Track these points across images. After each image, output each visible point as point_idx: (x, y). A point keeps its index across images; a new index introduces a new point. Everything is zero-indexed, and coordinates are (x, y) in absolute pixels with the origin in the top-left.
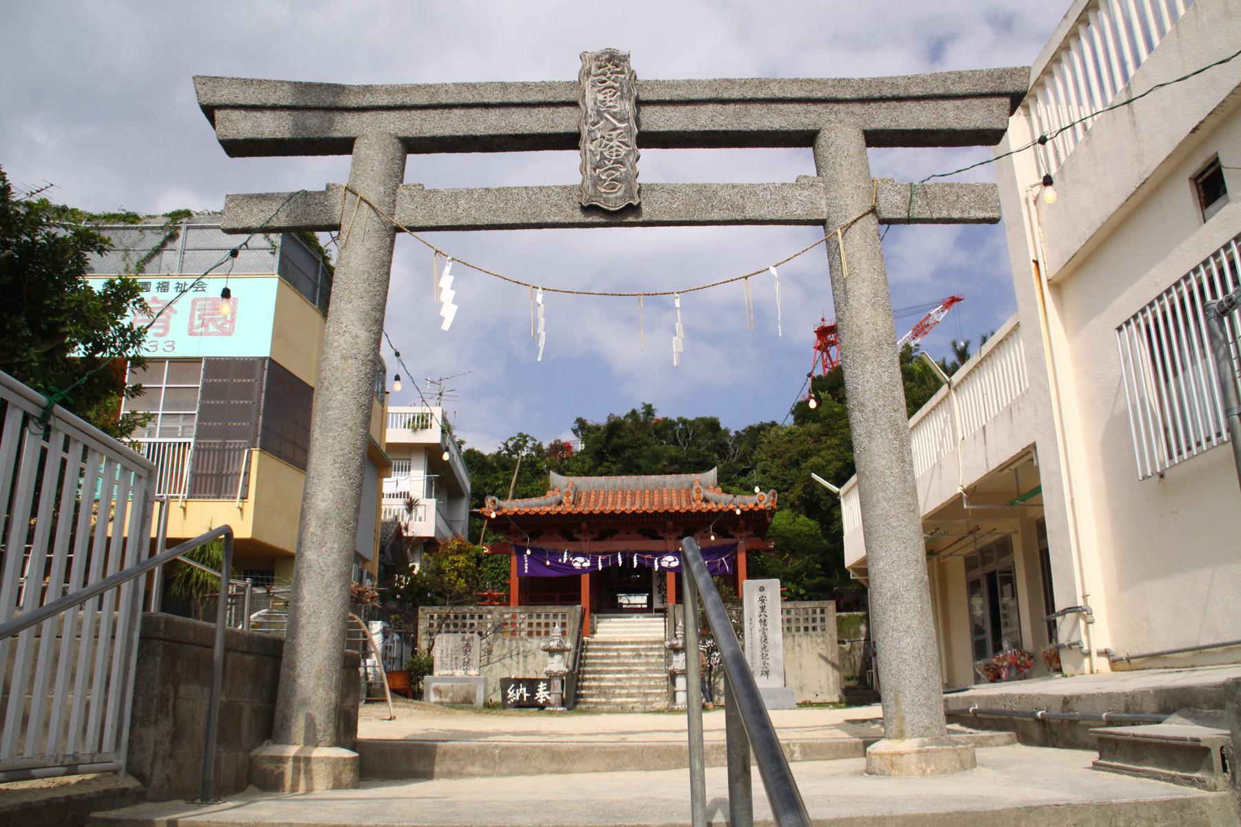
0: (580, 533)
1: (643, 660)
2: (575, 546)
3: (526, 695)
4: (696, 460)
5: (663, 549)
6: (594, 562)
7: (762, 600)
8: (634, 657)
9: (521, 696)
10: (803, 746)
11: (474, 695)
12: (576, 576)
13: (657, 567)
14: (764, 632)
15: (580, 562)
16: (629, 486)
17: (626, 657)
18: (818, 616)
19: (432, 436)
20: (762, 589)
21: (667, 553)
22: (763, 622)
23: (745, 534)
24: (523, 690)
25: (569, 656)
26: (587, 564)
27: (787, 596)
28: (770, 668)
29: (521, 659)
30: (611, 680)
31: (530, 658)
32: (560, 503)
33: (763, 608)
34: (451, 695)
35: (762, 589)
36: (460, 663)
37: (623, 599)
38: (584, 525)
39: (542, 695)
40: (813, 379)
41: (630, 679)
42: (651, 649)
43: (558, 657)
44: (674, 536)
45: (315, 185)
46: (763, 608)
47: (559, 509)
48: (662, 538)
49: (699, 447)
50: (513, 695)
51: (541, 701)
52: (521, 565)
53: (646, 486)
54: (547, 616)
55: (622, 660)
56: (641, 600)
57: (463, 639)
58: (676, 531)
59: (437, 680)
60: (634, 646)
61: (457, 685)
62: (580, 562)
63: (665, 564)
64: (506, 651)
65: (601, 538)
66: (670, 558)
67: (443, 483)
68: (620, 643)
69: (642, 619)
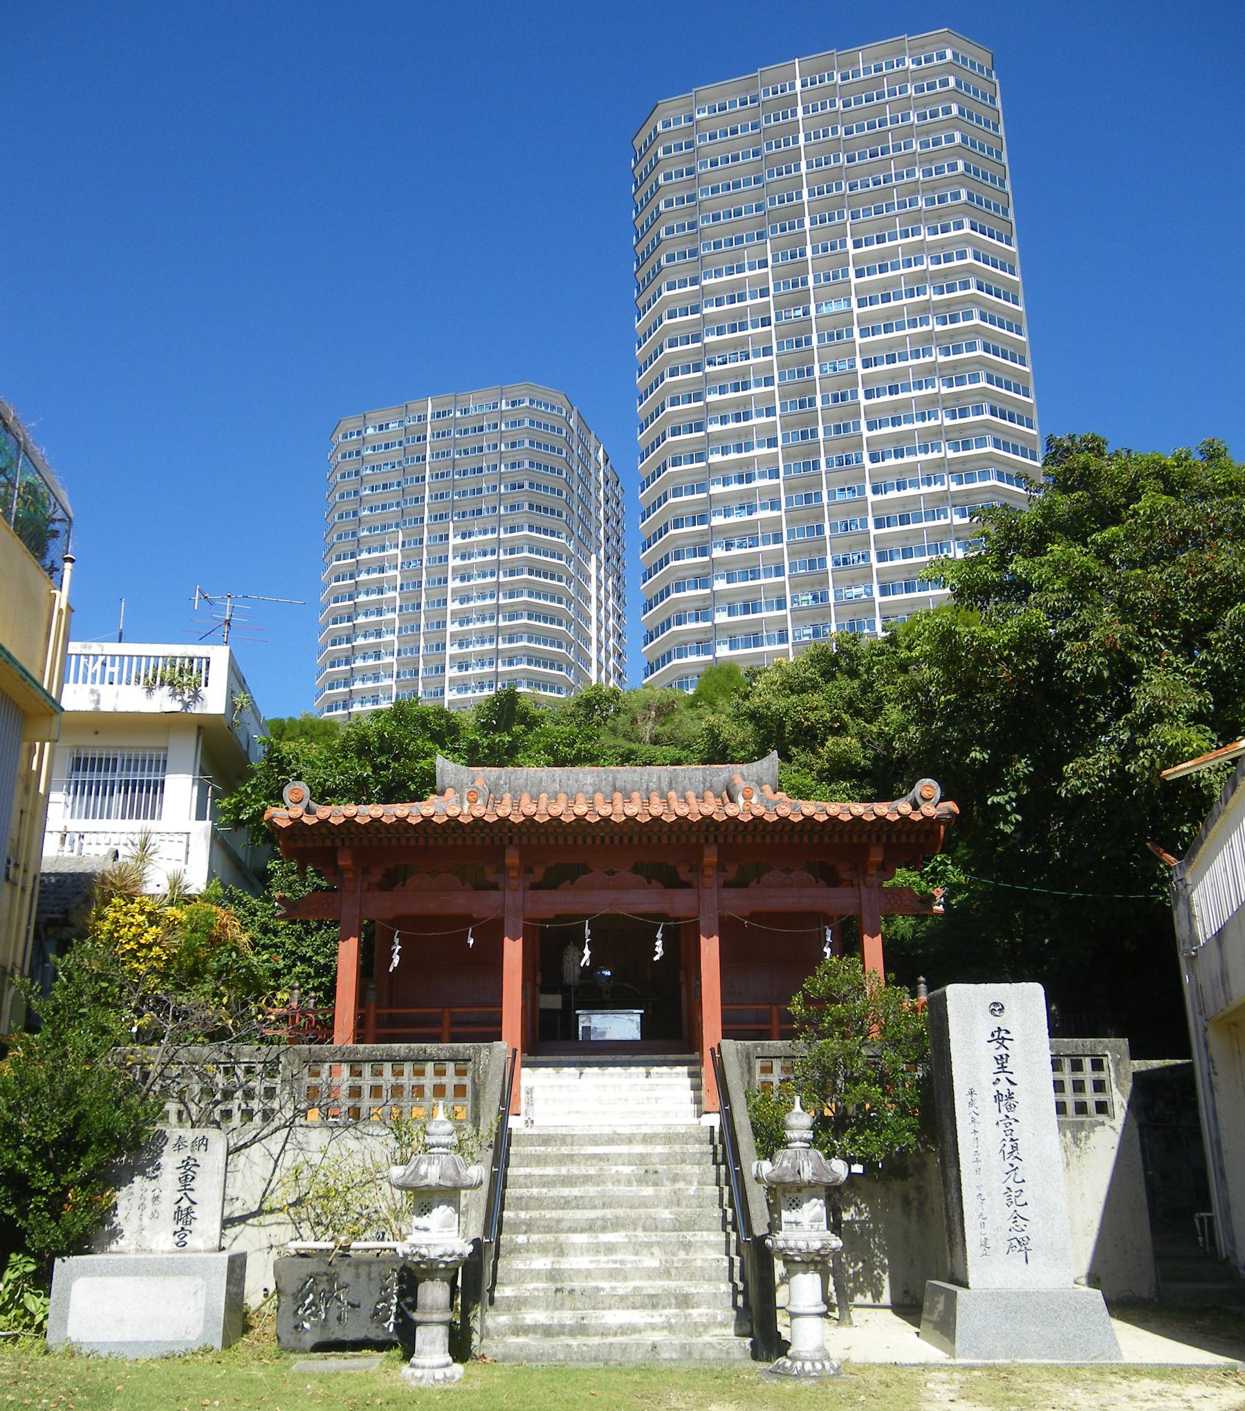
1: (666, 1189)
8: (642, 1181)
14: (1008, 1123)
18: (1088, 1075)
19: (214, 701)
20: (997, 1008)
22: (1005, 1099)
25: (474, 1203)
27: (1063, 1023)
33: (1002, 1061)
35: (997, 1008)
43: (442, 1213)
45: (613, 1240)
46: (1002, 1061)
60: (638, 1149)
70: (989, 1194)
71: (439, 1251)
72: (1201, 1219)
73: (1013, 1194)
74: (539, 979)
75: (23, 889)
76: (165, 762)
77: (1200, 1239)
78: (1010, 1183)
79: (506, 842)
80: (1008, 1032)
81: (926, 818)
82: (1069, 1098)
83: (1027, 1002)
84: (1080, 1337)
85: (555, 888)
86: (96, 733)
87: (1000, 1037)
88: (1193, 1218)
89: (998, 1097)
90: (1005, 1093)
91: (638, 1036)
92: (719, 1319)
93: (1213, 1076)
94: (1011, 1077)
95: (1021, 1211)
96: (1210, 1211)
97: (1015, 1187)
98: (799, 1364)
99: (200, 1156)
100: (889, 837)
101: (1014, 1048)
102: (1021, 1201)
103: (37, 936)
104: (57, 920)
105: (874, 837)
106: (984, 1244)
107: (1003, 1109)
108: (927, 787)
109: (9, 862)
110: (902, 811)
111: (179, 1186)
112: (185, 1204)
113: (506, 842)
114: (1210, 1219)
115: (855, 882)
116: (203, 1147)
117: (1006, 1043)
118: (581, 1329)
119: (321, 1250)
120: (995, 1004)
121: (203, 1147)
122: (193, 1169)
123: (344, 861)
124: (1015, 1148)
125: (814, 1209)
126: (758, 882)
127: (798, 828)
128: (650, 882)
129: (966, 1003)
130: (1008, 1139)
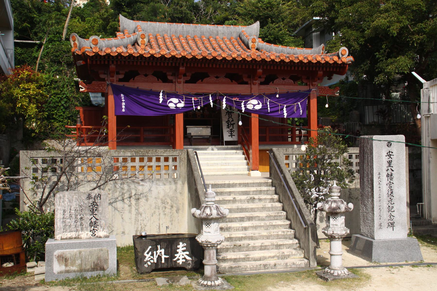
2: (168, 87)
3: (163, 257)
4: (179, 16)
5: (248, 93)
6: (188, 102)
7: (389, 154)
8: (248, 201)
9: (159, 258)
10: (212, 184)
11: (106, 260)
12: (171, 115)
13: (243, 109)
14: (390, 185)
15: (174, 103)
16: (188, 32)
17: (241, 201)
20: (389, 144)
21: (251, 96)
22: (390, 176)
24: (161, 251)
26: (181, 105)
28: (395, 220)
29: (133, 202)
30: (237, 229)
31: (142, 201)
32: (135, 43)
33: (390, 163)
34: (78, 262)
35: (389, 144)
36: (86, 223)
41: (255, 227)
42: (261, 192)
46: (390, 163)
47: (132, 51)
49: (181, 7)
50: (150, 258)
51: (180, 262)
52: (117, 106)
53: (202, 33)
54: (158, 160)
59: (59, 247)
61: (85, 251)
62: (174, 103)
63: (250, 107)
64: (117, 194)
65: (193, 80)
66: (255, 102)
68: (229, 186)
69: (216, 151)
72: (419, 205)
73: (390, 208)
77: (418, 211)
78: (390, 205)
80: (392, 153)
84: (411, 254)
85: (195, 82)
87: (389, 154)
89: (388, 175)
90: (390, 174)
91: (210, 134)
92: (293, 253)
93: (430, 158)
94: (392, 168)
95: (393, 214)
97: (391, 206)
98: (336, 272)
101: (394, 158)
106: (380, 225)
107: (389, 179)
110: (335, 60)
111: (90, 213)
112: (93, 220)
115: (308, 84)
116: (99, 198)
117: (392, 156)
121: (99, 198)
122: (96, 206)
124: (392, 193)
125: (341, 220)
130: (390, 189)
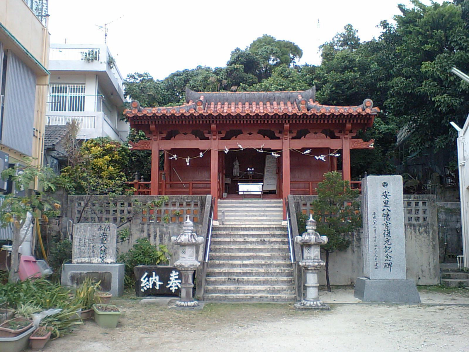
0: (209, 133)
3: (158, 283)
9: (154, 284)
14: (387, 225)
17: (251, 243)
19: (100, 66)
20: (385, 185)
22: (387, 216)
23: (349, 136)
33: (386, 203)
36: (97, 251)
37: (243, 188)
38: (213, 126)
39: (174, 283)
40: (37, 259)
44: (289, 136)
46: (386, 203)
48: (278, 138)
51: (173, 289)
55: (249, 246)
56: (256, 188)
57: (100, 229)
58: (291, 132)
67: (110, 99)
70: (379, 248)
71: (189, 264)
72: (459, 258)
74: (224, 172)
75: (39, 139)
76: (84, 89)
78: (386, 245)
79: (211, 122)
80: (388, 193)
81: (368, 114)
82: (413, 216)
83: (396, 182)
86: (59, 78)
88: (456, 258)
89: (384, 215)
94: (388, 208)
96: (463, 255)
99: (107, 232)
100: (353, 121)
102: (390, 250)
103: (45, 155)
104: (51, 148)
105: (348, 121)
108: (368, 102)
109: (34, 129)
112: (103, 248)
113: (211, 122)
114: (462, 258)
116: (108, 230)
117: (388, 196)
118: (237, 291)
119: (462, 248)
120: (385, 183)
121: (108, 230)
123: (153, 127)
124: (389, 233)
126: (305, 137)
127: (320, 117)
128: (264, 137)
129: (373, 184)
130: (386, 229)
